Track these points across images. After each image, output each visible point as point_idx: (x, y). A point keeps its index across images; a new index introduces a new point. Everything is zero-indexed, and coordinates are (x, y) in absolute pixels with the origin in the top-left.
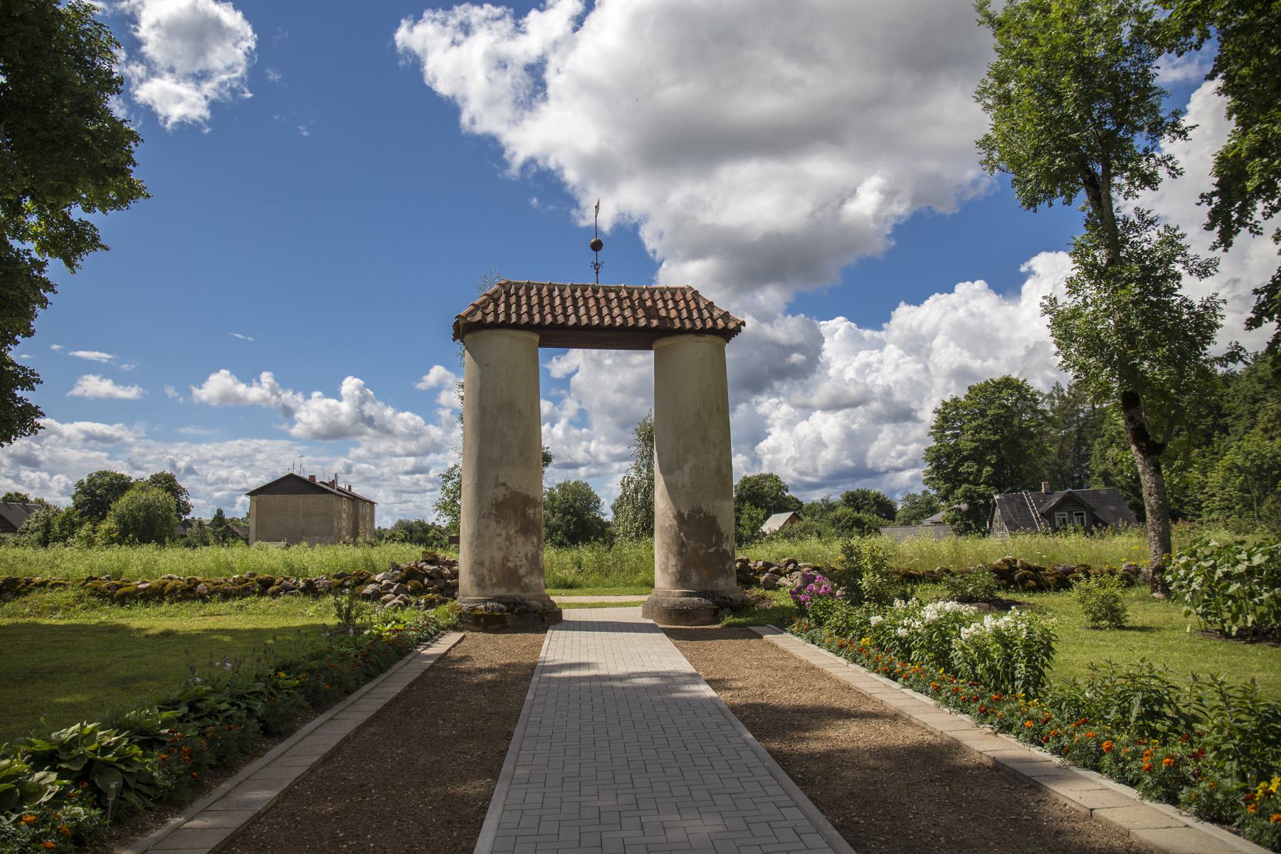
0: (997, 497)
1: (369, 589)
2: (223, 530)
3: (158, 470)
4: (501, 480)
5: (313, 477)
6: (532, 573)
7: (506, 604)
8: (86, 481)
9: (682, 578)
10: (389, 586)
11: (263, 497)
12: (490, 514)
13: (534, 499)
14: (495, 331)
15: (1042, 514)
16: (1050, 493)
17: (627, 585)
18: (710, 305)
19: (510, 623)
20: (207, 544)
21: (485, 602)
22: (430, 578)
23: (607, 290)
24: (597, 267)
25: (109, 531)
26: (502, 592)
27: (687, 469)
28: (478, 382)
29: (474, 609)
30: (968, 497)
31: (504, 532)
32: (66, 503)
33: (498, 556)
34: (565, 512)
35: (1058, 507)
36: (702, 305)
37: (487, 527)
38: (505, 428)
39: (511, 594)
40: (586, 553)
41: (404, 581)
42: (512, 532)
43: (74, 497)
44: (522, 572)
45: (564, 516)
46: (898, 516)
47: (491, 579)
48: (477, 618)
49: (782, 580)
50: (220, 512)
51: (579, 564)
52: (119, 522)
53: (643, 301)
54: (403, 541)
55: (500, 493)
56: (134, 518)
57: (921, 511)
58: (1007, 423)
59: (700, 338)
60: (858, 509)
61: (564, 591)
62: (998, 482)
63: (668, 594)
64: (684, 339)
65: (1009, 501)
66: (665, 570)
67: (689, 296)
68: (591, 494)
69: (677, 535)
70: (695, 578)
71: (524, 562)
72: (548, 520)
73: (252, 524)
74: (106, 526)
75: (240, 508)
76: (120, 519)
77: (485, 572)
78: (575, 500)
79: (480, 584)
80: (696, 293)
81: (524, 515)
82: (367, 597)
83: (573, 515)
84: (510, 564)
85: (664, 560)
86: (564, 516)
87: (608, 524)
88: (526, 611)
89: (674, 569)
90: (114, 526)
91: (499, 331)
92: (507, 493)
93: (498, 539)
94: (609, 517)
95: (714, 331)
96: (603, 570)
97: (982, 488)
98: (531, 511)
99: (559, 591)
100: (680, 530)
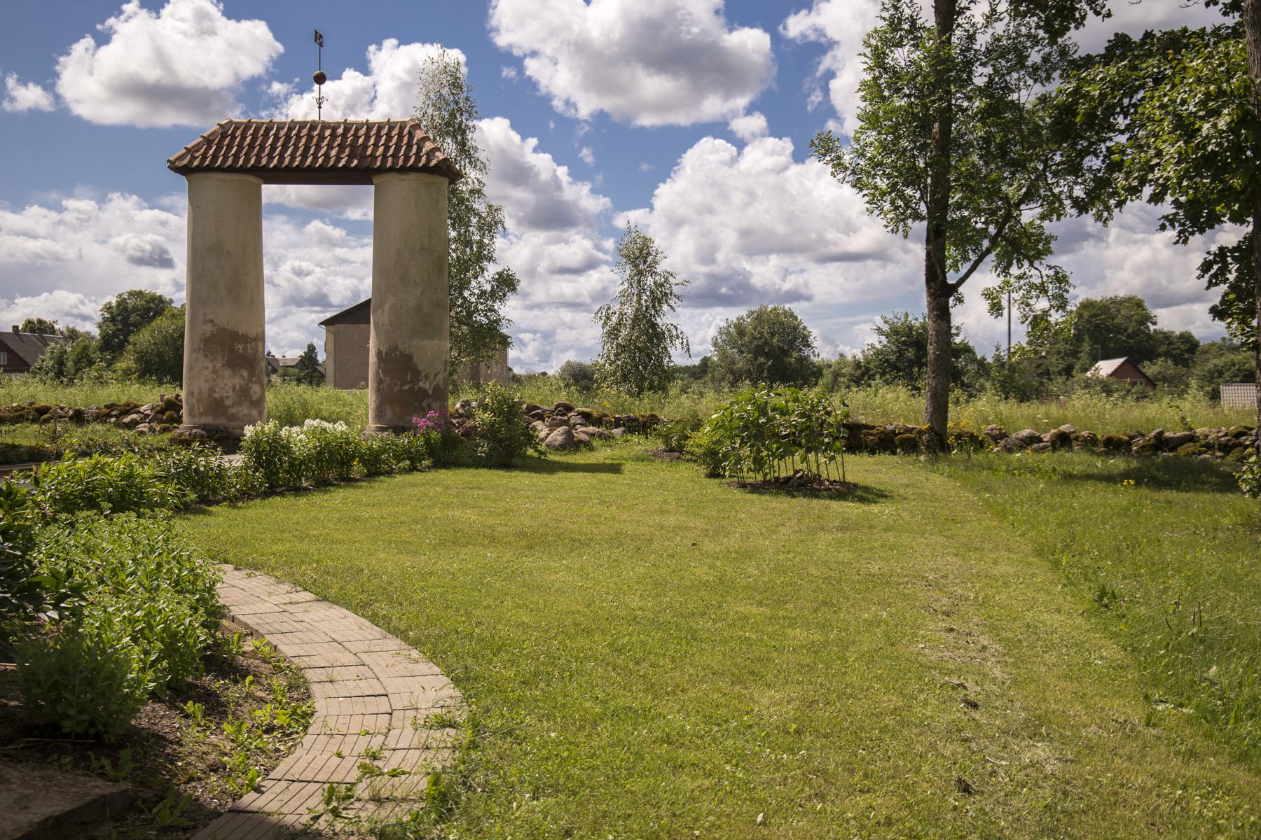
1: (127, 420)
4: (209, 317)
6: (240, 404)
8: (114, 304)
11: (342, 327)
26: (207, 420)
27: (386, 308)
31: (211, 366)
32: (92, 329)
33: (205, 387)
34: (758, 351)
39: (216, 422)
41: (162, 412)
43: (100, 327)
44: (228, 402)
54: (299, 381)
55: (208, 329)
59: (403, 177)
71: (231, 393)
78: (773, 335)
79: (191, 414)
81: (232, 350)
83: (768, 356)
84: (216, 395)
92: (215, 329)
93: (205, 372)
98: (240, 347)
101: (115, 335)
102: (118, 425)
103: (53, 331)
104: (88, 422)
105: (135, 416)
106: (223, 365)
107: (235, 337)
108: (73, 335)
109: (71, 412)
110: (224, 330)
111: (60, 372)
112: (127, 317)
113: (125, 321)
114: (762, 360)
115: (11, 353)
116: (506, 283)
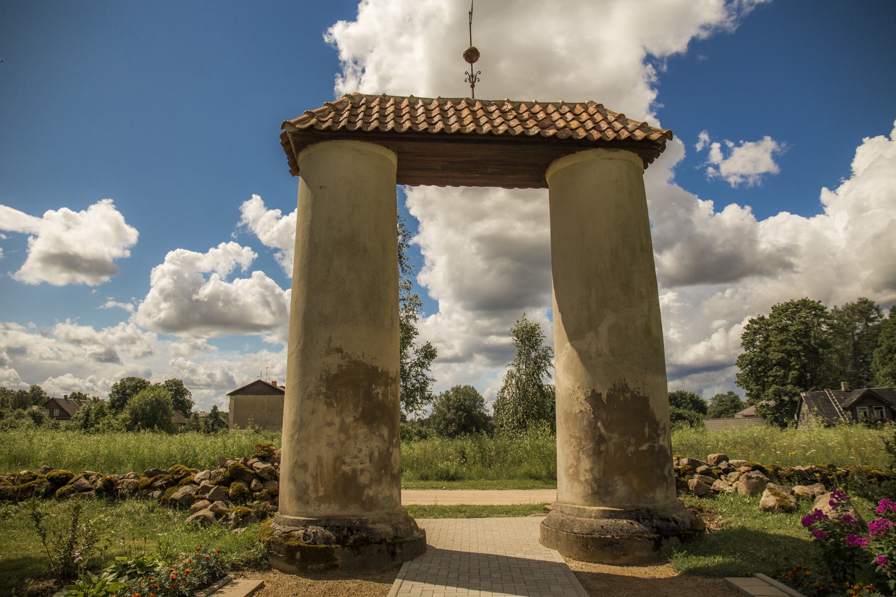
0: (803, 395)
1: (178, 494)
2: (215, 422)
3: (170, 378)
4: (336, 344)
5: (275, 383)
6: (379, 481)
7: (337, 529)
9: (600, 490)
10: (206, 489)
11: (239, 396)
12: (318, 394)
13: (385, 374)
14: (333, 143)
15: (844, 409)
16: (849, 391)
17: (511, 477)
18: (621, 118)
19: (340, 561)
20: (198, 430)
21: (306, 524)
22: (262, 480)
23: (485, 104)
24: (472, 80)
25: (124, 420)
27: (603, 329)
28: (309, 212)
29: (288, 536)
30: (777, 394)
31: (337, 420)
32: (105, 395)
33: (328, 455)
34: (458, 409)
35: (859, 402)
36: (611, 118)
37: (313, 412)
38: (352, 285)
39: (345, 513)
40: (467, 444)
41: (226, 482)
42: (349, 420)
44: (363, 479)
45: (457, 412)
46: (709, 410)
47: (316, 490)
48: (291, 551)
49: (718, 484)
50: (215, 408)
51: (463, 455)
52: (132, 414)
53: (534, 115)
55: (334, 362)
56: (143, 410)
57: (728, 407)
58: (806, 335)
60: (678, 406)
61: (446, 483)
62: (801, 382)
63: (581, 512)
64: (590, 155)
65: (814, 398)
66: (575, 477)
67: (592, 110)
68: (477, 395)
69: (593, 426)
70: (621, 489)
71: (367, 464)
72: (445, 415)
73: (231, 417)
74: (123, 416)
75: (224, 406)
76: (134, 413)
77: (309, 480)
78: (465, 400)
79: (301, 496)
80: (599, 107)
81: (369, 395)
82: (174, 504)
84: (346, 469)
85: (572, 461)
86: (457, 412)
87: (490, 418)
88: (366, 542)
89: (589, 476)
90: (128, 416)
91: (340, 143)
92: (344, 363)
93: (328, 431)
94: (491, 412)
95: (630, 144)
96: (486, 461)
97: (789, 387)
98: (380, 390)
99: (441, 483)
100: (596, 418)
101: (118, 400)
102: (166, 503)
103: (85, 398)
104: (123, 497)
105: (187, 489)
106: (356, 420)
107: (375, 375)
108: (96, 400)
109: (99, 483)
110: (358, 364)
111: (87, 425)
112: (125, 391)
113: (124, 393)
114: (461, 413)
115: (62, 409)
116: (429, 353)
